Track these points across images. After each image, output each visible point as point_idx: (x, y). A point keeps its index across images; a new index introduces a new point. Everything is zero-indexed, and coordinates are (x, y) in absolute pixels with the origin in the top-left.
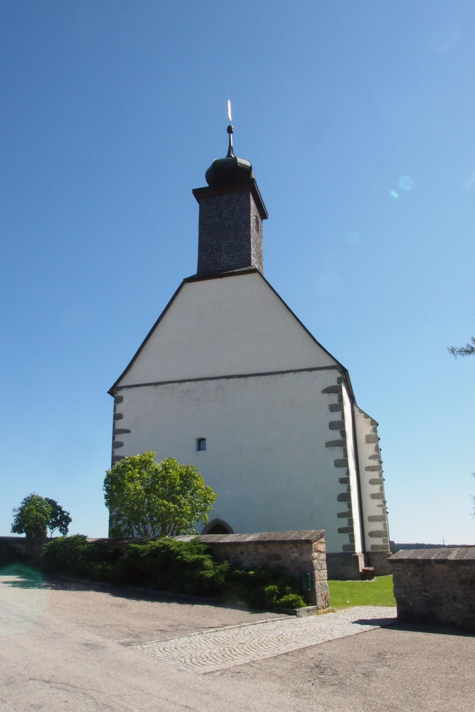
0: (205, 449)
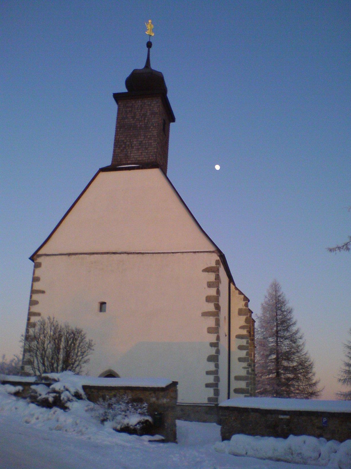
0: (105, 311)
